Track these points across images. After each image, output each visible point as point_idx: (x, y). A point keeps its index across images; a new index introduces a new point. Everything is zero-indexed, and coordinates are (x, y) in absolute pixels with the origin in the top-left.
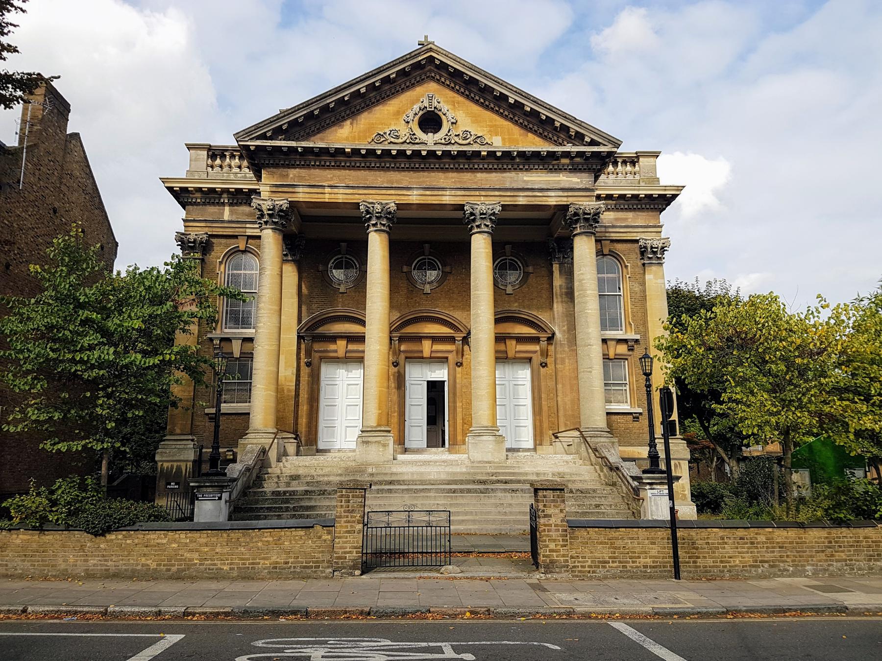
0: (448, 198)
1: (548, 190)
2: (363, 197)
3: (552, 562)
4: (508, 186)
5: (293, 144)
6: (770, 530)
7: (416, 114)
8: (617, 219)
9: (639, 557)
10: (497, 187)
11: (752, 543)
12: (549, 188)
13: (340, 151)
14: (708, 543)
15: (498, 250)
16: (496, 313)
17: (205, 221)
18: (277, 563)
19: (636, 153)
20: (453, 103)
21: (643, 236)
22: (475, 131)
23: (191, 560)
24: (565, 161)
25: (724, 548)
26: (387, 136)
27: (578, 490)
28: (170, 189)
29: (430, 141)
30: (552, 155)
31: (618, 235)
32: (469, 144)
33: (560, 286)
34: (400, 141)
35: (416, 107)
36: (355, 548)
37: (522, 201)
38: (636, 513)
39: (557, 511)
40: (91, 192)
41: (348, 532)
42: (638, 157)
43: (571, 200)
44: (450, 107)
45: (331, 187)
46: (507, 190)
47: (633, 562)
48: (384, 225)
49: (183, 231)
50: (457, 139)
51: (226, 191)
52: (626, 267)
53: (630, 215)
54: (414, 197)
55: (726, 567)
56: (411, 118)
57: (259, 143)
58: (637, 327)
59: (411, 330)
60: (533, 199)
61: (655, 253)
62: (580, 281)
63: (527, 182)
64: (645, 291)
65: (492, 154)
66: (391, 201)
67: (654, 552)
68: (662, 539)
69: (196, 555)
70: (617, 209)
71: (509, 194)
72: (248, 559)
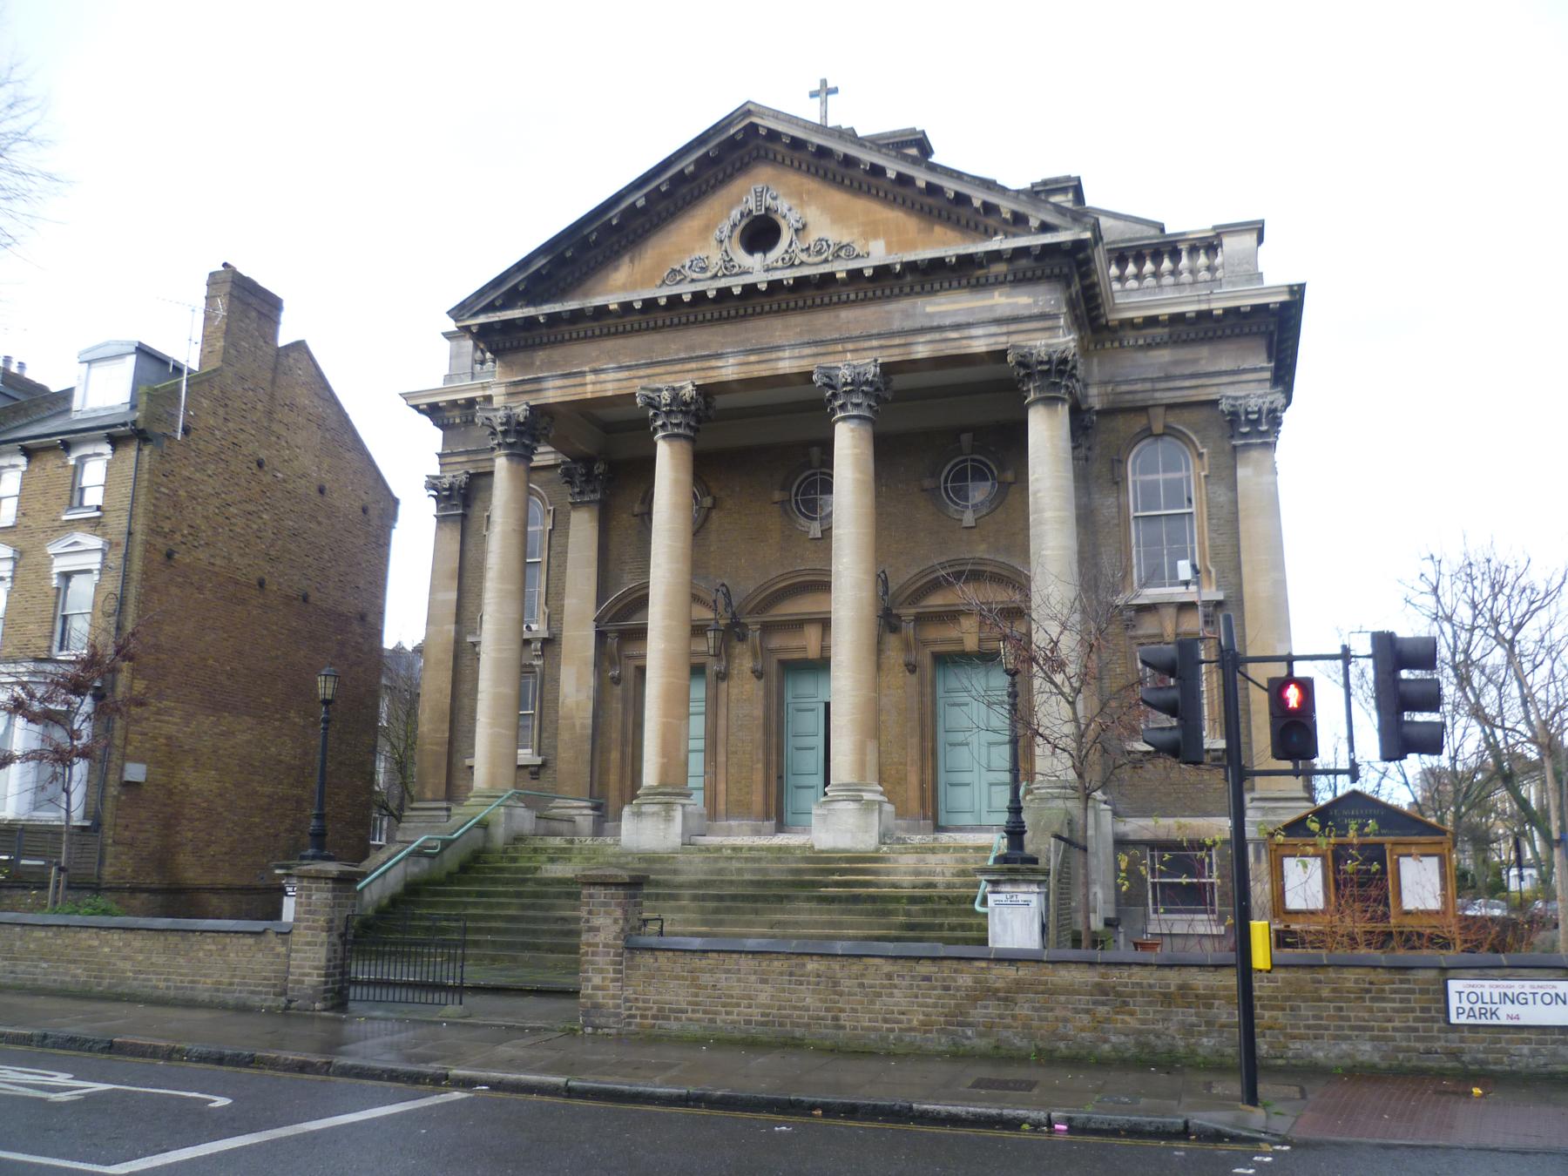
0: (787, 364)
1: (969, 325)
2: (644, 382)
3: (596, 1006)
4: (896, 326)
5: (530, 311)
6: (984, 964)
7: (735, 225)
8: (1176, 363)
9: (738, 1005)
10: (874, 331)
11: (947, 988)
12: (974, 322)
13: (602, 311)
14: (862, 985)
15: (888, 452)
17: (467, 452)
18: (220, 983)
19: (1215, 228)
21: (1231, 391)
22: (835, 235)
23: (124, 972)
25: (891, 995)
26: (687, 272)
27: (940, 898)
28: (416, 407)
29: (757, 269)
30: (966, 261)
31: (1178, 393)
32: (826, 261)
34: (709, 274)
35: (735, 214)
36: (316, 968)
37: (922, 351)
39: (609, 921)
41: (308, 944)
42: (1218, 236)
43: (1014, 339)
44: (794, 202)
45: (595, 371)
46: (892, 334)
47: (727, 1013)
48: (857, 405)
49: (437, 473)
50: (804, 257)
51: (454, 403)
52: (1200, 455)
53: (1204, 351)
54: (729, 369)
55: (892, 1030)
56: (726, 232)
57: (482, 319)
58: (1221, 574)
59: (936, 601)
60: (943, 346)
61: (1250, 422)
62: (1035, 493)
63: (931, 316)
64: (1236, 502)
65: (750, 290)
67: (763, 998)
68: (781, 974)
69: (128, 965)
70: (1175, 342)
71: (897, 341)
72: (186, 975)
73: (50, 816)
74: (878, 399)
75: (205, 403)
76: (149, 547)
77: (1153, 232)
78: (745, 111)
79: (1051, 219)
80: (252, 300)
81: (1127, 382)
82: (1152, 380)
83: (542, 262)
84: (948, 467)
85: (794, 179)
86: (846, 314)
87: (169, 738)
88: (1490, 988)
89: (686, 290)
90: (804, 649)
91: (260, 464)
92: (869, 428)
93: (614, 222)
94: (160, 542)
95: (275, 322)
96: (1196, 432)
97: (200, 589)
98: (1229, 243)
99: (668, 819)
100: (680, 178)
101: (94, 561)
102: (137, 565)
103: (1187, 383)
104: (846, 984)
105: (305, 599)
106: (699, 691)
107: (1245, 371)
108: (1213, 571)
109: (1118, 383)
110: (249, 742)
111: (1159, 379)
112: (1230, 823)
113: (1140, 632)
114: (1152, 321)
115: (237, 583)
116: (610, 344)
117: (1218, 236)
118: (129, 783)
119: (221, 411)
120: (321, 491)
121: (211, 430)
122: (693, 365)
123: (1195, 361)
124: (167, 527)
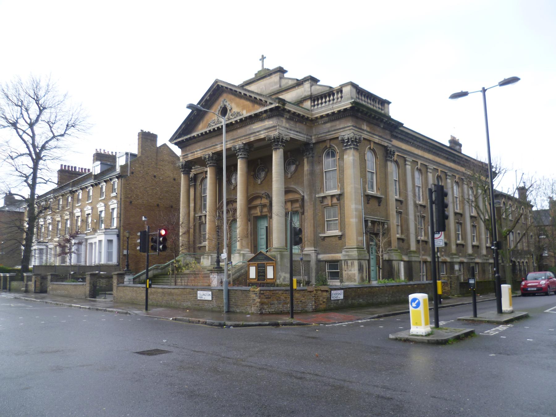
8: (331, 127)
16: (285, 188)
20: (230, 100)
24: (264, 115)
38: (26, 200)
42: (342, 87)
45: (196, 151)
53: (337, 122)
73: (110, 263)
74: (248, 152)
75: (137, 165)
76: (125, 201)
78: (216, 82)
79: (271, 102)
83: (183, 126)
89: (211, 129)
90: (257, 213)
91: (155, 176)
92: (244, 160)
94: (128, 200)
96: (337, 146)
97: (140, 209)
99: (208, 259)
100: (207, 100)
102: (123, 206)
103: (333, 133)
106: (249, 223)
111: (327, 132)
112: (57, 264)
113: (324, 204)
114: (322, 117)
116: (199, 144)
117: (342, 87)
119: (142, 166)
120: (174, 179)
123: (335, 126)
124: (129, 196)
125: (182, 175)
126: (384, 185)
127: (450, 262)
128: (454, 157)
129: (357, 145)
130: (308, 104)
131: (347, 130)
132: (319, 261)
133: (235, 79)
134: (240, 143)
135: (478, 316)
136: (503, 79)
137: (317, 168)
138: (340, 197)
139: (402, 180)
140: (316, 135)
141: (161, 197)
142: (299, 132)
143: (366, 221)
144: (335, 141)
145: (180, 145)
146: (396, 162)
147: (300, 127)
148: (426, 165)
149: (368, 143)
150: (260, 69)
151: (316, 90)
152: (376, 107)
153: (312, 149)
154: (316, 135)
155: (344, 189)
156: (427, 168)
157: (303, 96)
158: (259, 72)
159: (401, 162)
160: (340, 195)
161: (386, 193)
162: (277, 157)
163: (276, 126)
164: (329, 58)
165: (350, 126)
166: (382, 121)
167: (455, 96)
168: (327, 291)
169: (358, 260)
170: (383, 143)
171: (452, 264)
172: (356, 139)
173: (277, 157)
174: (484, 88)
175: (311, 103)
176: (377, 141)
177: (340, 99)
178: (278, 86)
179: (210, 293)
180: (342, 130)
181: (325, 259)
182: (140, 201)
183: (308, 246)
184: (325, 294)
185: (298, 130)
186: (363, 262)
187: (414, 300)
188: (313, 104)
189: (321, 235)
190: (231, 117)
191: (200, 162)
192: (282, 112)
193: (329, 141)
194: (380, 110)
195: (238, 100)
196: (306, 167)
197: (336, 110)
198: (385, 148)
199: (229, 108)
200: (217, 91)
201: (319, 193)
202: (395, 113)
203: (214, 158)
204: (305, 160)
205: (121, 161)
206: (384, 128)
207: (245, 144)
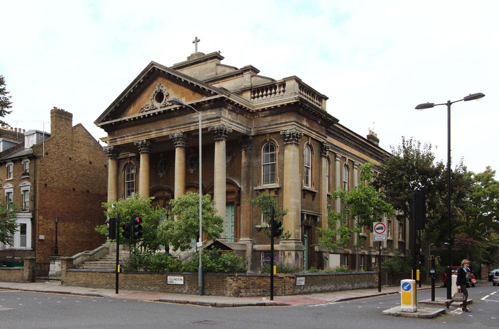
8: (272, 121)
19: (283, 79)
20: (167, 85)
24: (207, 105)
29: (159, 107)
33: (245, 162)
40: (94, 145)
45: (127, 136)
46: (186, 124)
53: (279, 117)
54: (153, 135)
66: (143, 138)
70: (272, 115)
74: (186, 142)
75: (52, 146)
77: (270, 81)
78: (152, 64)
80: (63, 116)
81: (260, 127)
82: (266, 126)
84: (265, 145)
85: (167, 81)
86: (177, 119)
87: (51, 229)
88: (173, 277)
91: (70, 159)
92: (183, 149)
93: (118, 106)
95: (72, 122)
98: (288, 84)
101: (29, 188)
104: (94, 277)
105: (88, 192)
107: (288, 122)
108: (278, 179)
109: (258, 128)
110: (74, 229)
114: (263, 110)
115: (66, 190)
118: (40, 240)
119: (57, 147)
120: (91, 163)
121: (54, 152)
122: (146, 134)
123: (277, 120)
124: (44, 178)
125: (110, 160)
126: (318, 182)
127: (367, 255)
128: (377, 154)
129: (298, 141)
130: (248, 95)
131: (289, 125)
132: (254, 251)
133: (168, 61)
134: (178, 131)
135: (436, 299)
136: (468, 95)
137: (255, 161)
138: (278, 191)
139: (332, 176)
140: (255, 128)
141: (76, 181)
142: (240, 125)
143: (302, 215)
144: (276, 136)
145: (105, 128)
146: (328, 158)
147: (241, 119)
148: (353, 161)
149: (306, 138)
150: (194, 52)
151: (257, 82)
152: (315, 102)
153: (250, 142)
154: (255, 128)
155: (283, 183)
156: (353, 165)
157: (243, 87)
158: (192, 55)
159: (332, 157)
160: (278, 188)
161: (319, 187)
162: (220, 149)
163: (220, 117)
164: (267, 47)
165: (292, 121)
166: (320, 117)
167: (421, 107)
168: (293, 278)
169: (296, 251)
170: (319, 139)
171: (369, 257)
172: (297, 134)
173: (220, 149)
174: (449, 101)
175: (251, 95)
176: (314, 137)
177: (282, 93)
178: (215, 73)
179: (182, 278)
180: (283, 125)
181: (260, 249)
182: (56, 184)
183: (244, 236)
184: (292, 280)
185: (239, 122)
186: (299, 252)
187: (405, 284)
188: (252, 96)
189: (257, 226)
190: (168, 103)
191: (130, 147)
192: (226, 103)
193: (268, 135)
194: (318, 106)
195: (176, 86)
196: (244, 160)
197: (279, 105)
198: (321, 144)
199: (165, 94)
200: (152, 74)
201: (256, 186)
202: (331, 108)
203: (147, 145)
204: (243, 153)
205: (30, 142)
206: (321, 124)
207: (184, 133)
